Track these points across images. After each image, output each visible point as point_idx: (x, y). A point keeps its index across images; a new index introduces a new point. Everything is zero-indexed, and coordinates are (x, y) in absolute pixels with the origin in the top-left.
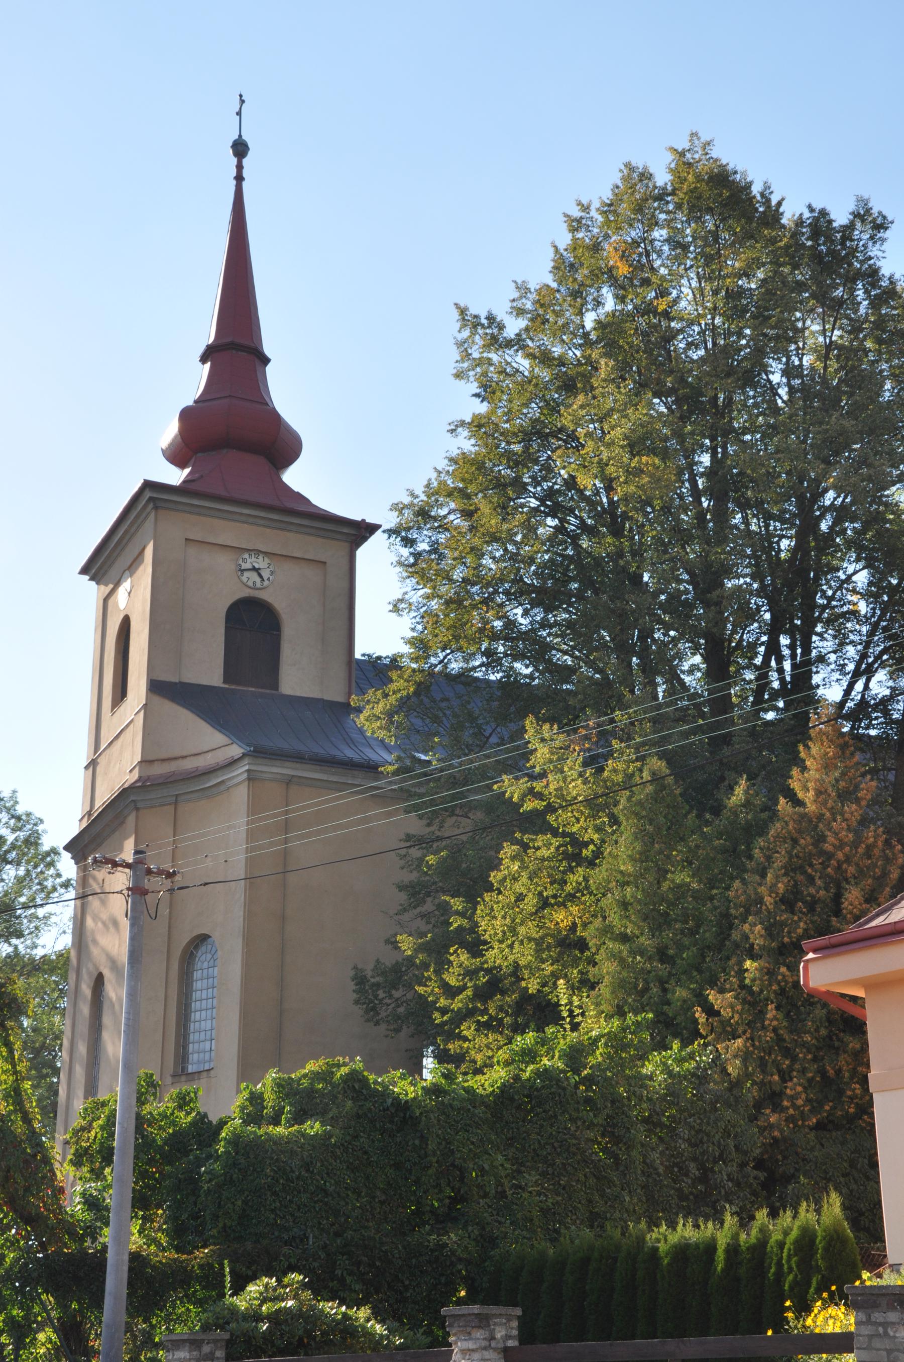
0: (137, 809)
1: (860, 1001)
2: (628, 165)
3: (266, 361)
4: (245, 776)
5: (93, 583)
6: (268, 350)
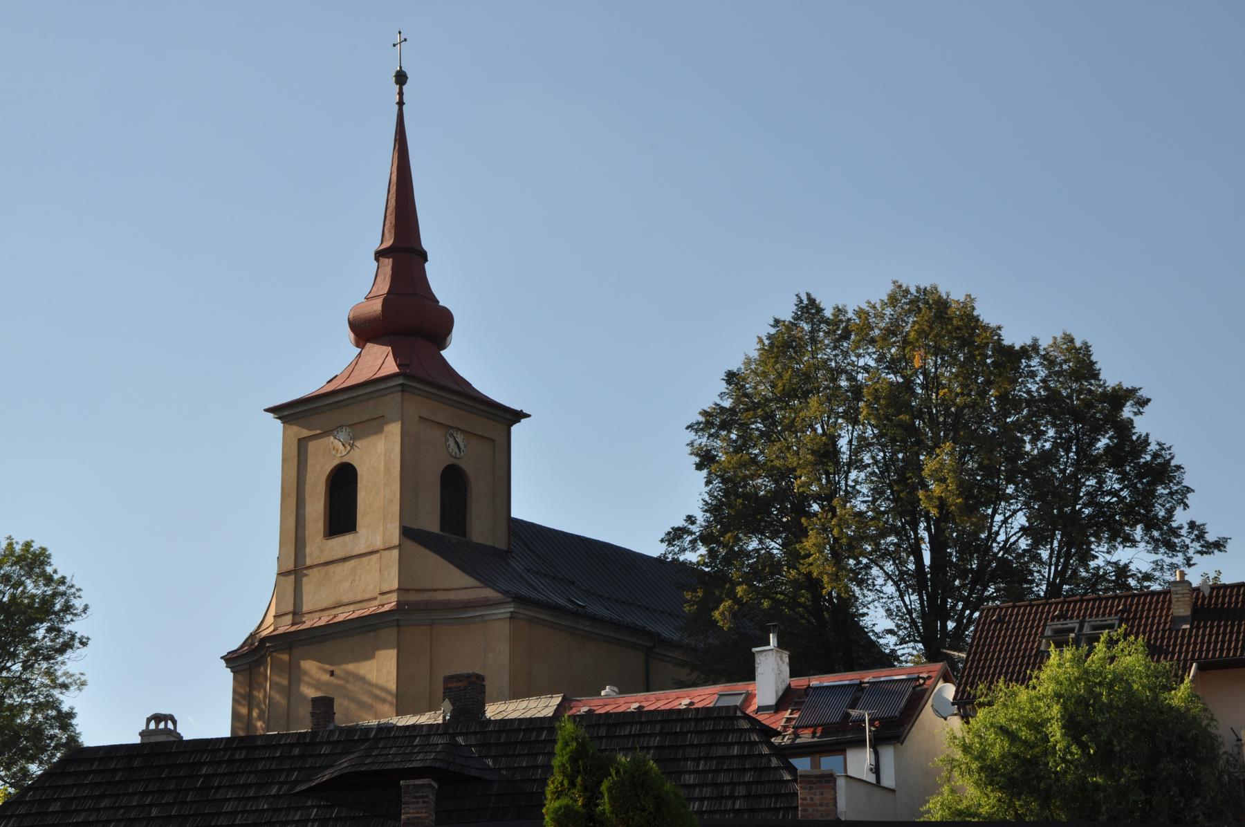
0: (398, 626)
2: (999, 328)
3: (423, 256)
5: (279, 421)
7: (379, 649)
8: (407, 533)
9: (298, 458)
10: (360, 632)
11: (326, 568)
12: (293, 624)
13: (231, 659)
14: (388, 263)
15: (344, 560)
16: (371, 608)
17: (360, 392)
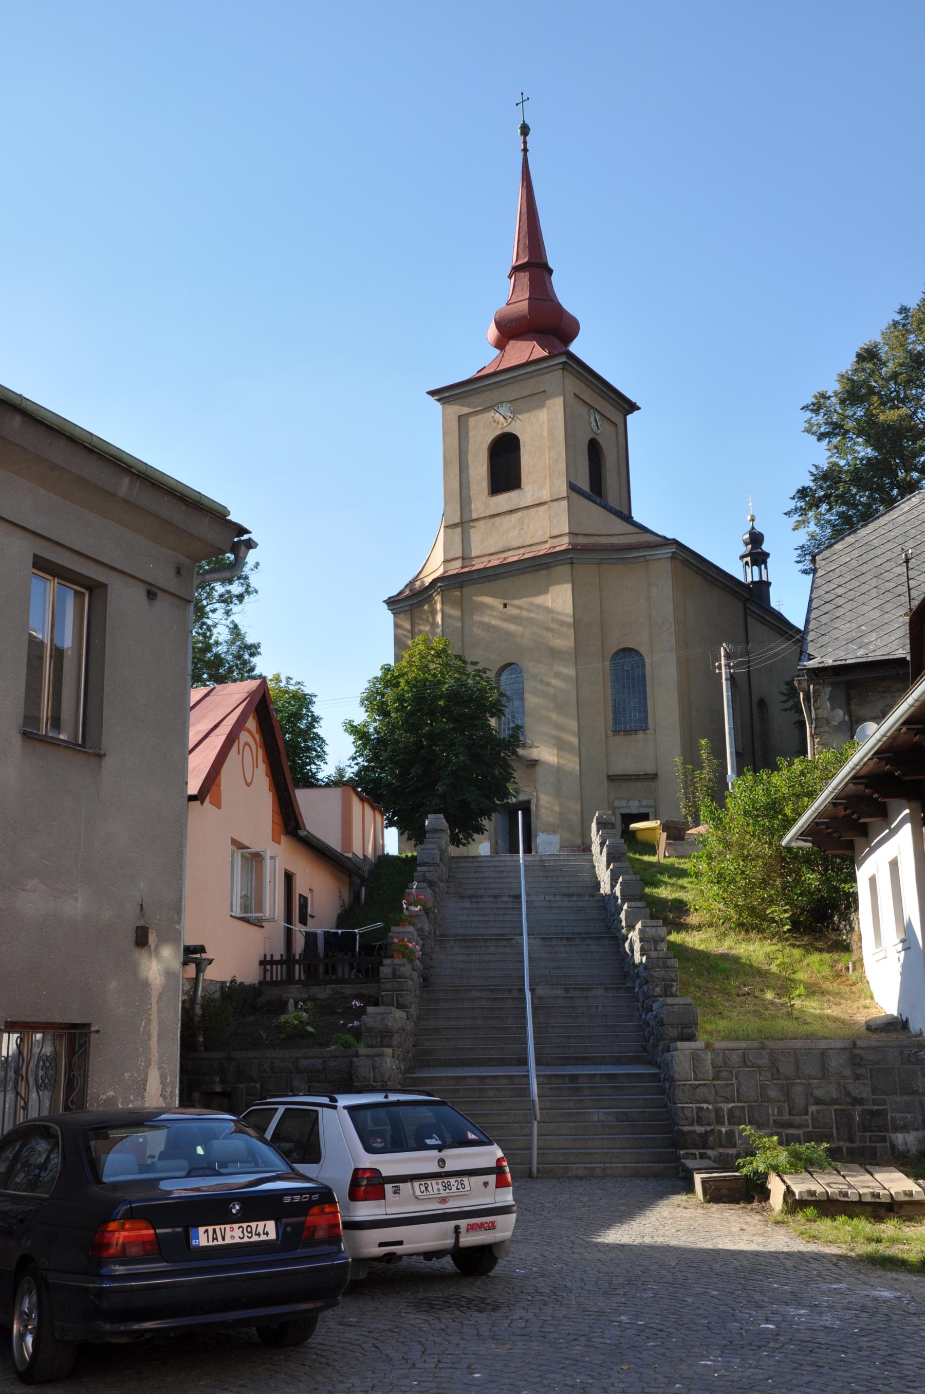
0: (572, 563)
1: (187, 1006)
3: (550, 271)
4: (670, 555)
6: (551, 264)
7: (552, 584)
8: (572, 487)
9: (461, 431)
10: (537, 568)
11: (492, 520)
12: (462, 568)
13: (392, 603)
14: (525, 277)
15: (511, 512)
16: (543, 550)
17: (522, 372)
